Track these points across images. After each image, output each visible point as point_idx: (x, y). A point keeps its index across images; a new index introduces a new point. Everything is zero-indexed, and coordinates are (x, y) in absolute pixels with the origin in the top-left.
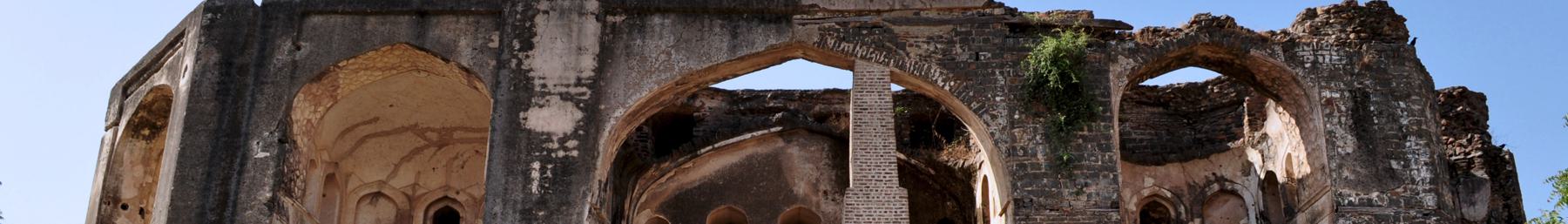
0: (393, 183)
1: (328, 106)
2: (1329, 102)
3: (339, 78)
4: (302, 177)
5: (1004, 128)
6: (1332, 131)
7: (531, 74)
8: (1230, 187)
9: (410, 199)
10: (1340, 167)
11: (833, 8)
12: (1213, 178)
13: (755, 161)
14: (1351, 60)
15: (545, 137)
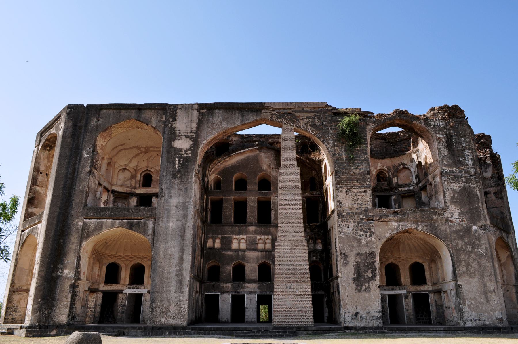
0: (129, 165)
2: (439, 138)
7: (176, 129)
9: (135, 170)
11: (275, 107)
12: (401, 164)
13: (249, 158)
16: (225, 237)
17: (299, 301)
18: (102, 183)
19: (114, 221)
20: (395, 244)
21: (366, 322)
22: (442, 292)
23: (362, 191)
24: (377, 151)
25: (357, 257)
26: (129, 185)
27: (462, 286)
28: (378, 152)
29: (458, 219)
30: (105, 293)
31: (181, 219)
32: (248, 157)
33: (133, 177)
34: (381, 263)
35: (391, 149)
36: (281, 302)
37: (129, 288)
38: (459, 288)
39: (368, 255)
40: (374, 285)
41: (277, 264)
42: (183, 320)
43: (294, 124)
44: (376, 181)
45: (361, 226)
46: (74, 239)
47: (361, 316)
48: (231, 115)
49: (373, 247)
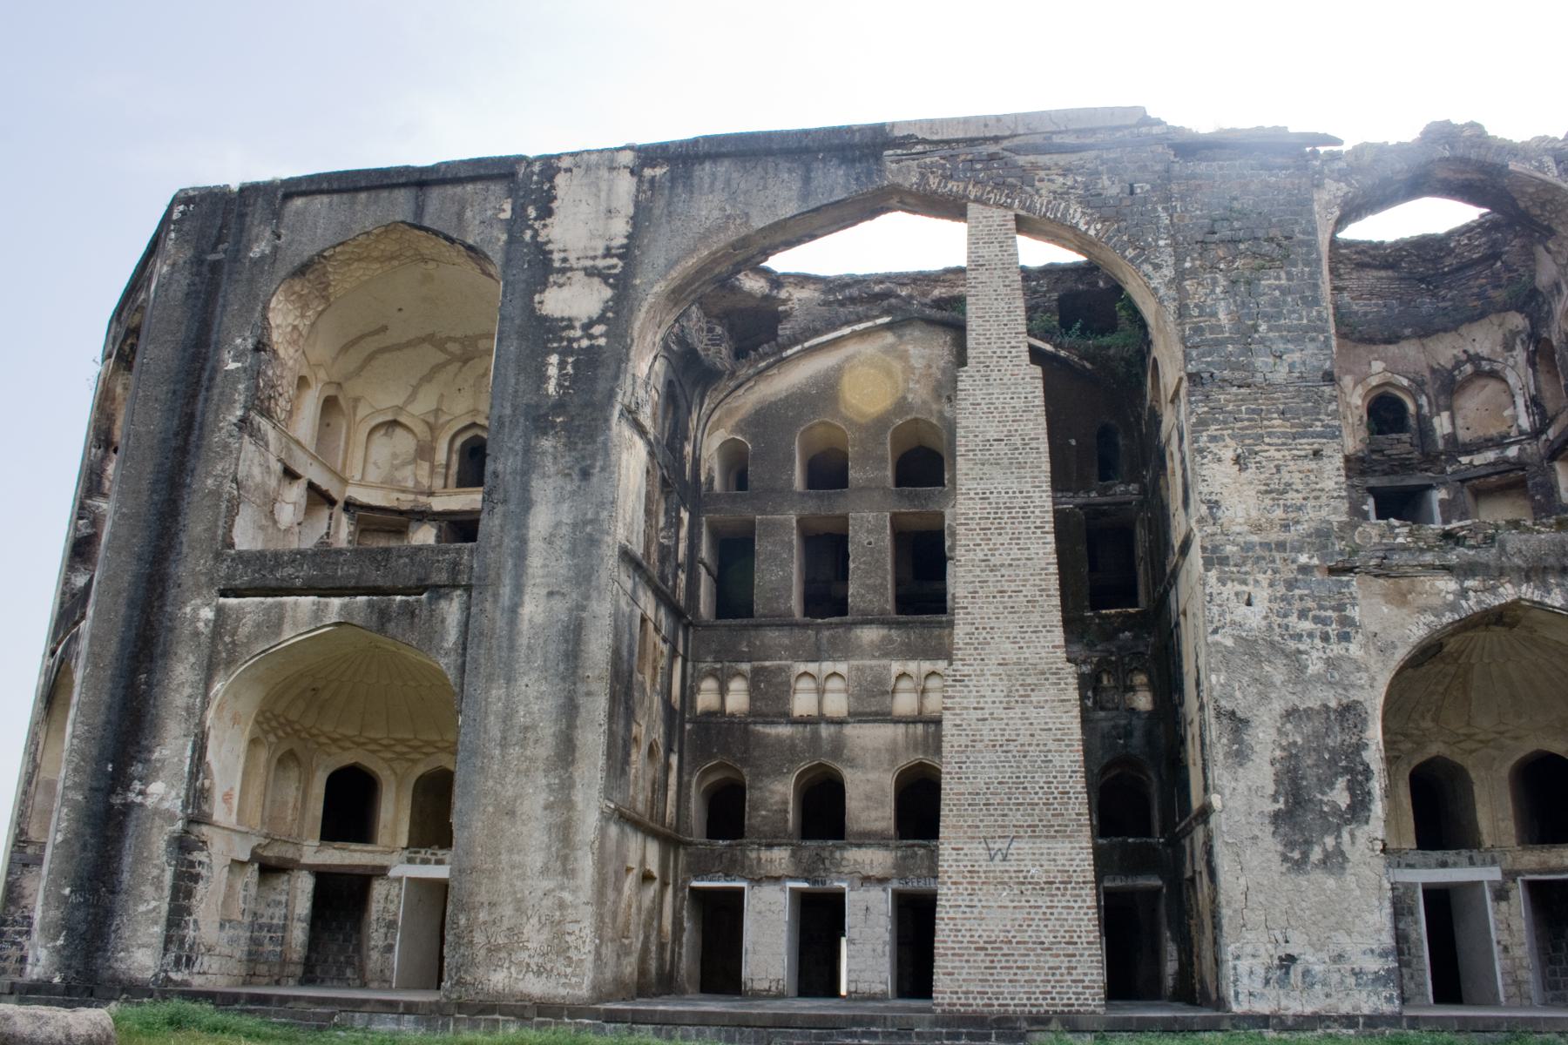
0: (409, 408)
1: (320, 309)
3: (327, 272)
4: (286, 395)
5: (1172, 281)
7: (550, 247)
8: (1487, 368)
9: (432, 428)
11: (935, 138)
12: (1464, 357)
16: (765, 669)
17: (1041, 911)
18: (300, 471)
19: (323, 600)
21: (1328, 996)
23: (1303, 453)
24: (1366, 314)
25: (1289, 726)
26: (410, 484)
28: (1370, 316)
31: (565, 589)
33: (424, 452)
34: (1391, 760)
35: (1423, 303)
36: (968, 915)
37: (410, 861)
39: (1333, 717)
41: (949, 763)
42: (574, 980)
43: (1014, 199)
44: (1363, 433)
45: (1301, 598)
46: (183, 671)
47: (1306, 973)
48: (762, 178)
49: (1353, 686)
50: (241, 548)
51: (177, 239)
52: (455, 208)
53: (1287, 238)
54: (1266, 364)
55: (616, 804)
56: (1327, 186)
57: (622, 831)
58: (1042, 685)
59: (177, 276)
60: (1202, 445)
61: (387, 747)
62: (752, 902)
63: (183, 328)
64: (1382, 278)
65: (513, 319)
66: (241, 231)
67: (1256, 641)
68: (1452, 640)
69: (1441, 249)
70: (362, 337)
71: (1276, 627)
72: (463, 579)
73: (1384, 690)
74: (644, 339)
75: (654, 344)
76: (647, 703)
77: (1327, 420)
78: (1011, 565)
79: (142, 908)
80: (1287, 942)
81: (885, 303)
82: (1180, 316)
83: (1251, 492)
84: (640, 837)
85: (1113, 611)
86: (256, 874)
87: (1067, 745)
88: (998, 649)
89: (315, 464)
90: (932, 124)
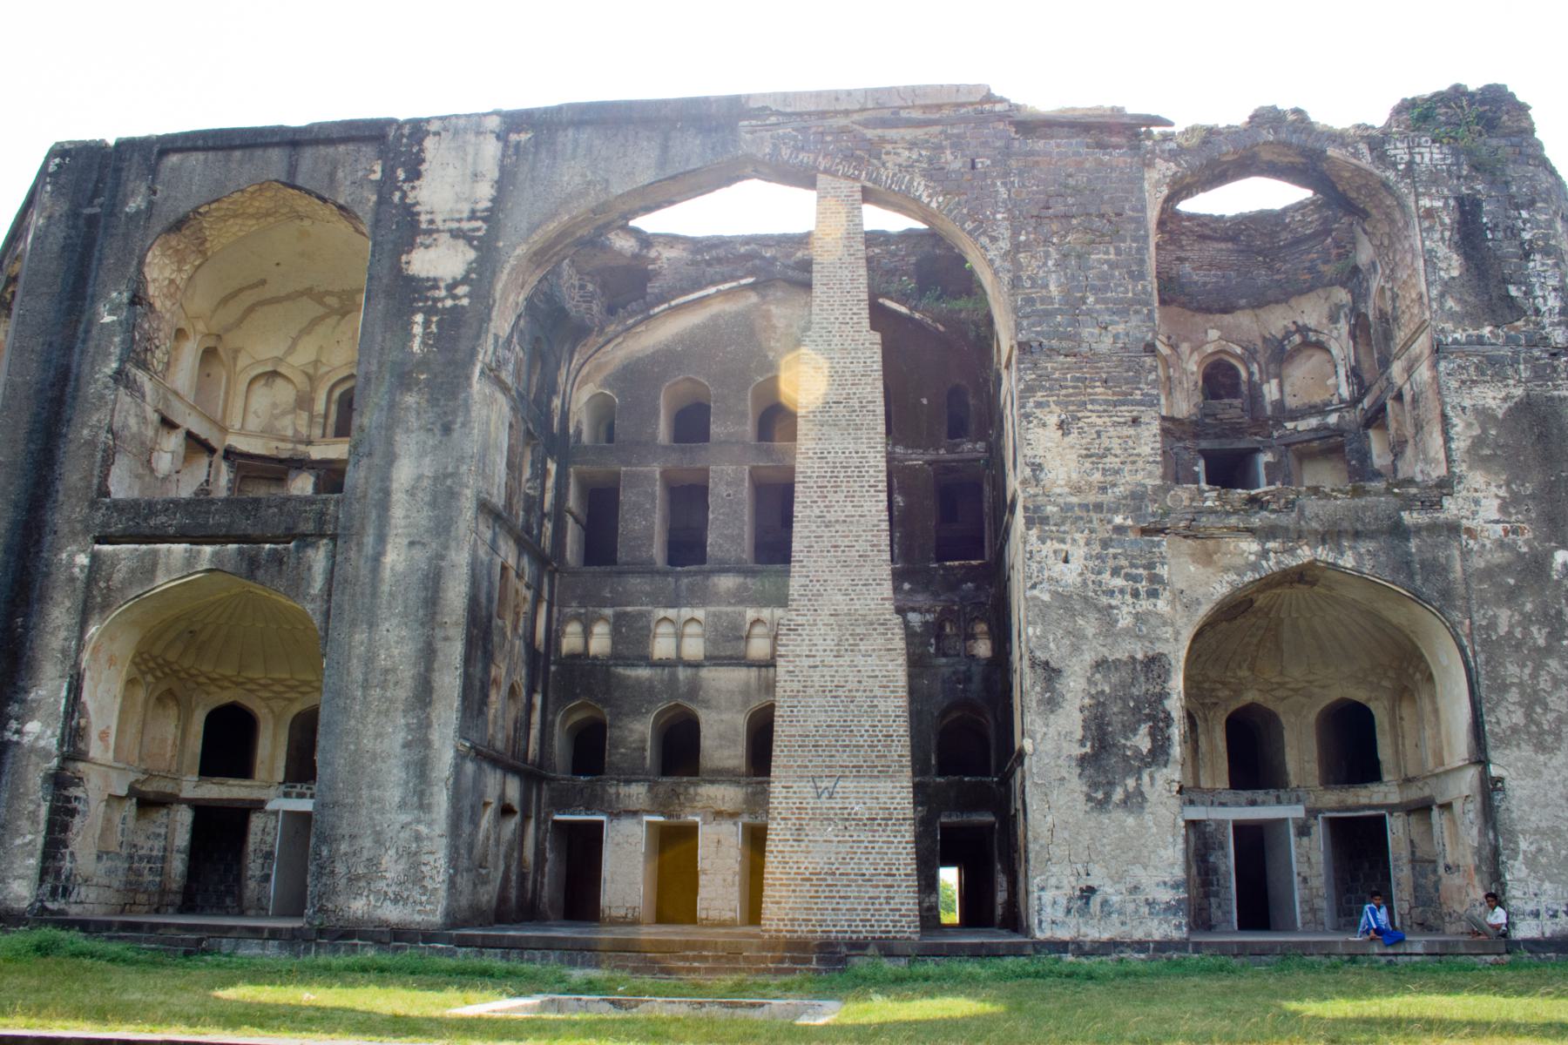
0: (290, 359)
1: (197, 263)
2: (1430, 213)
4: (163, 347)
5: (1007, 253)
6: (1432, 250)
7: (418, 208)
8: (1314, 339)
9: (310, 378)
10: (1442, 295)
11: (789, 110)
12: (1293, 328)
13: (721, 321)
14: (1458, 159)
15: (430, 283)
16: (626, 614)
17: (862, 845)
18: (177, 421)
19: (195, 547)
20: (1261, 632)
21: (1123, 923)
22: (1434, 807)
23: (1122, 420)
24: (1205, 284)
25: (1098, 676)
26: (290, 433)
27: (1506, 782)
28: (1209, 286)
29: (1497, 522)
30: (204, 813)
32: (713, 325)
33: (304, 402)
35: (1259, 275)
36: (796, 849)
37: (287, 795)
38: (1495, 789)
39: (1139, 668)
40: (1160, 781)
41: (782, 707)
42: (428, 907)
43: (861, 171)
44: (1198, 398)
45: (1115, 557)
46: (59, 615)
47: (1105, 903)
48: (623, 145)
49: (1158, 639)
50: (117, 497)
51: (52, 192)
52: (327, 169)
53: (1118, 215)
54: (1092, 334)
55: (472, 742)
56: (1158, 166)
57: (480, 768)
58: (870, 635)
59: (53, 229)
60: (1028, 410)
61: (265, 686)
62: (612, 834)
63: (59, 280)
64: (1222, 250)
65: (380, 278)
66: (118, 185)
67: (1071, 596)
68: (1261, 596)
69: (1277, 224)
70: (241, 290)
71: (1090, 583)
72: (329, 529)
73: (1187, 643)
74: (506, 299)
75: (517, 304)
76: (507, 646)
77: (1146, 388)
78: (845, 521)
79: (19, 841)
80: (1088, 874)
81: (749, 264)
82: (1014, 287)
83: (1072, 456)
84: (499, 774)
85: (957, 563)
86: (134, 809)
87: (892, 692)
88: (830, 600)
89: (194, 414)
90: (785, 97)
